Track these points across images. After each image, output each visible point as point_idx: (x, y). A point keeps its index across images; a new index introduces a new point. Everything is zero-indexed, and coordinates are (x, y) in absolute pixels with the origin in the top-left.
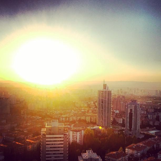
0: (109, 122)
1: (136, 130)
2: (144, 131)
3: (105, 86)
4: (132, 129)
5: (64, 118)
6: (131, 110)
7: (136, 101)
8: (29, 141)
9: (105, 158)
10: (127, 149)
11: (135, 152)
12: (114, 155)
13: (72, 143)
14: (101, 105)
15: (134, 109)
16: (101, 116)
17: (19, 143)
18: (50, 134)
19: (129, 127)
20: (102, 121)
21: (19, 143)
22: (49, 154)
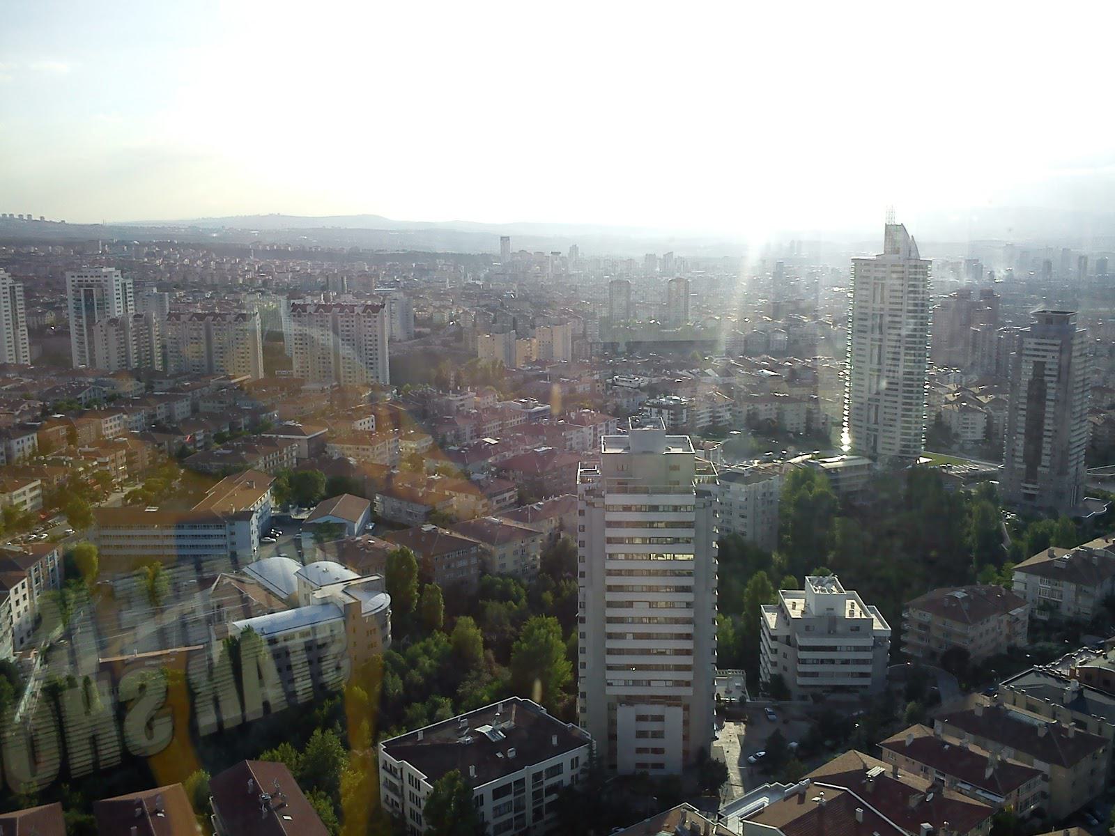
0: (913, 432)
1: (1062, 472)
2: (1103, 480)
3: (894, 233)
4: (1039, 469)
5: (665, 412)
6: (1039, 367)
7: (1067, 319)
8: (500, 524)
9: (905, 620)
10: (1018, 576)
11: (1068, 589)
12: (1049, 726)
13: (5, 738)
14: (868, 341)
15: (1054, 379)
16: (868, 429)
17: (440, 530)
18: (625, 491)
19: (1026, 457)
20: (876, 430)
21: (454, 535)
22: (620, 588)
